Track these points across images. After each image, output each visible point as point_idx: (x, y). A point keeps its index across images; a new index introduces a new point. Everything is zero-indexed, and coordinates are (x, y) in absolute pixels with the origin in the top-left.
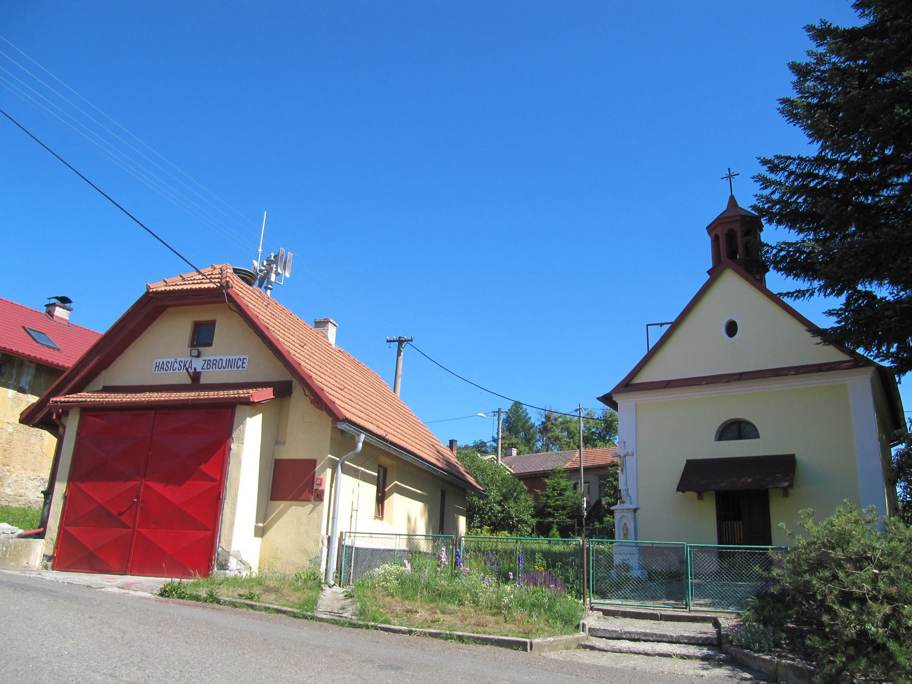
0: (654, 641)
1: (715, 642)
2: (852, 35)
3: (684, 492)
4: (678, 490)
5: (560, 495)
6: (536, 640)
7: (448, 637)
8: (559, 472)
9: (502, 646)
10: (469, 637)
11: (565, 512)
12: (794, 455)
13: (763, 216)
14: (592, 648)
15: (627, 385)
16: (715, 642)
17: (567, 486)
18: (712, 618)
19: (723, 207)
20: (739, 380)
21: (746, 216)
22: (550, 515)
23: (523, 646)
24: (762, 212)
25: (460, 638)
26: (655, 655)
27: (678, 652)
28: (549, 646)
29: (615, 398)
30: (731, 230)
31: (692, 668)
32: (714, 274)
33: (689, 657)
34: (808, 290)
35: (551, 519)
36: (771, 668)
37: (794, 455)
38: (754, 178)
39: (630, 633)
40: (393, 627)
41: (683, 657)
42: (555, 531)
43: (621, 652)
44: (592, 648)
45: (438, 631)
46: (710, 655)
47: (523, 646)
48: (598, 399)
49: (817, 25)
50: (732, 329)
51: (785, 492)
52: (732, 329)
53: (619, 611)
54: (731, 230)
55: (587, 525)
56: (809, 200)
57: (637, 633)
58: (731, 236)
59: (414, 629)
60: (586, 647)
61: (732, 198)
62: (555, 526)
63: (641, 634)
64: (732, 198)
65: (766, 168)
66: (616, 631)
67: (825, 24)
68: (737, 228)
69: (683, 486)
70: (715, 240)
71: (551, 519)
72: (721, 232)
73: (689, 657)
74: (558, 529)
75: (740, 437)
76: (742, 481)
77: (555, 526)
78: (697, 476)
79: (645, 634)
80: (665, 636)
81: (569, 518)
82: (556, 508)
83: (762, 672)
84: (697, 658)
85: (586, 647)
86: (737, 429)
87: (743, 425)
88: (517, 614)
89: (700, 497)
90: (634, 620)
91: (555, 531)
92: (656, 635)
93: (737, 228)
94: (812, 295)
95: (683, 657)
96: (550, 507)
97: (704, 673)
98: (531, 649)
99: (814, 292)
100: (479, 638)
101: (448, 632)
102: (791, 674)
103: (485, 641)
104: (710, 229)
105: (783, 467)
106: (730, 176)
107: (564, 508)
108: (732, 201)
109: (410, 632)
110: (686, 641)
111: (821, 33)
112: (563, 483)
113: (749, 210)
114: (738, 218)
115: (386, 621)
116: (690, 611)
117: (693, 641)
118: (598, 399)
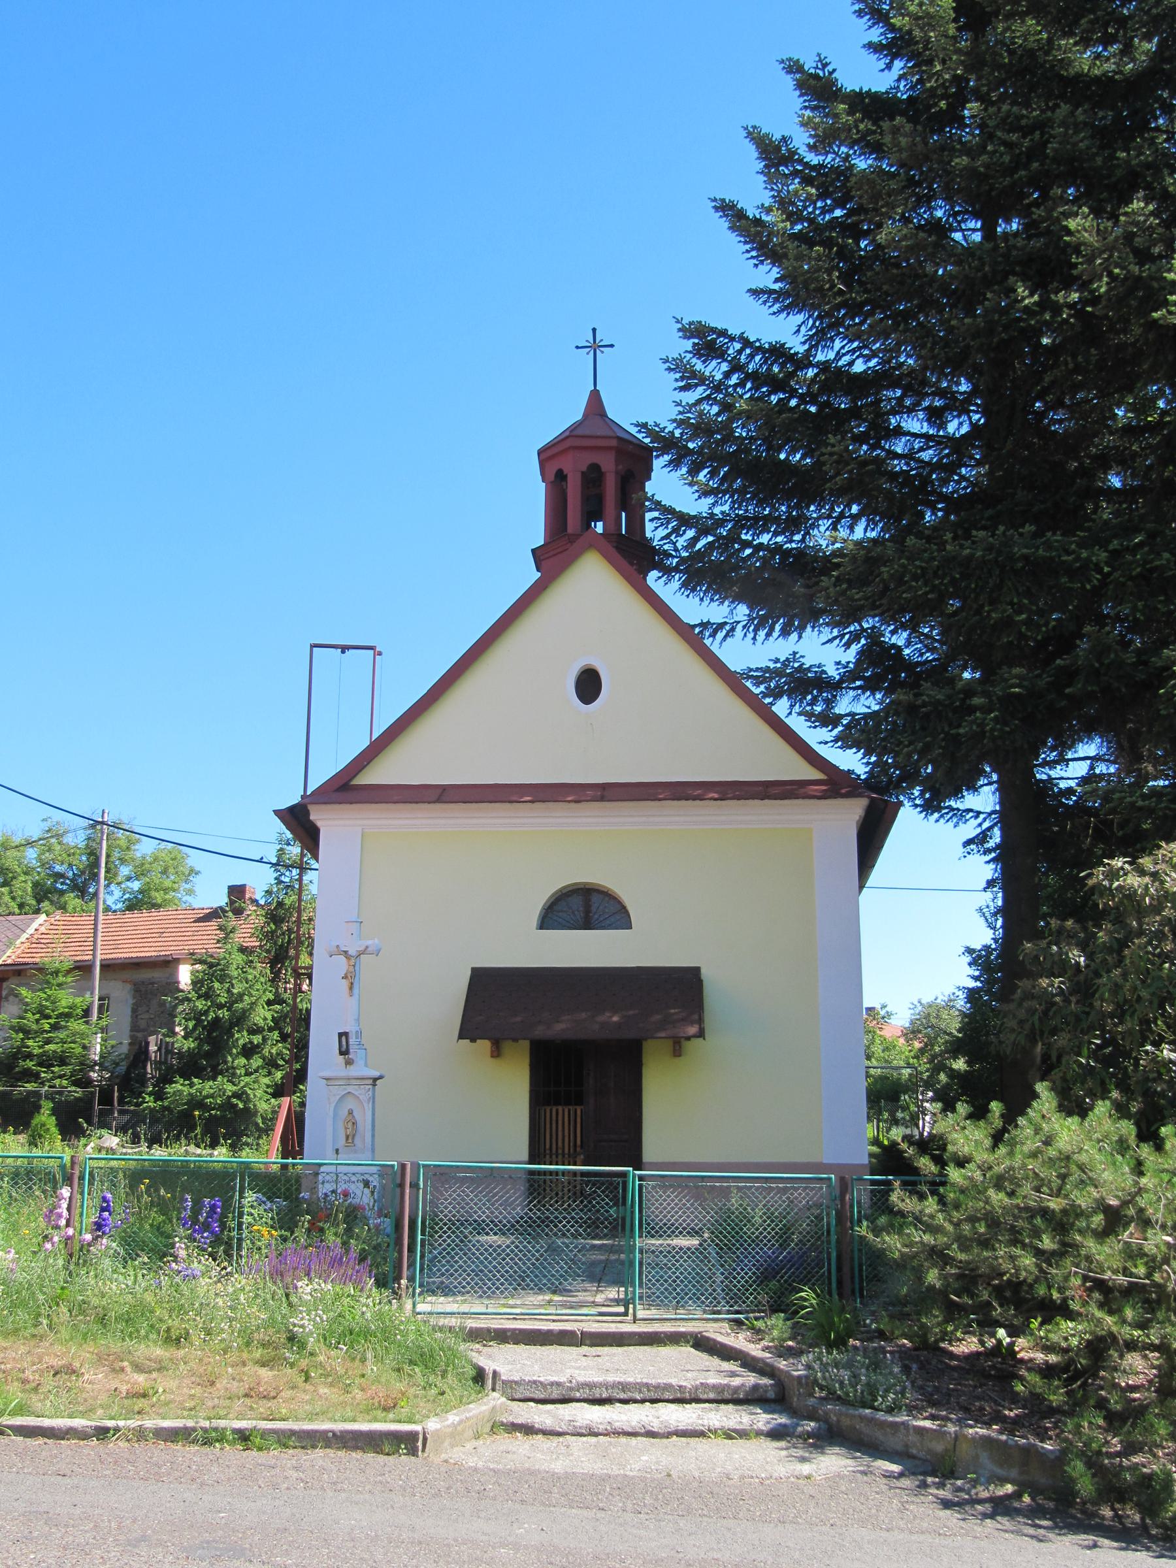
0: (643, 1401)
1: (771, 1395)
2: (872, 106)
3: (473, 1040)
4: (461, 1036)
5: (55, 1027)
6: (432, 1425)
7: (210, 1438)
8: (56, 973)
9: (356, 1448)
10: (265, 1434)
11: (67, 1070)
12: (697, 970)
13: (664, 451)
14: (528, 1430)
15: (344, 788)
16: (771, 1395)
17: (72, 1007)
18: (691, 1334)
19: (575, 413)
20: (602, 799)
21: (630, 442)
22: (33, 1076)
23: (408, 1443)
24: (667, 444)
25: (244, 1437)
26: (668, 1435)
27: (717, 1424)
28: (452, 1435)
29: (317, 815)
30: (595, 468)
31: (771, 1461)
32: (552, 559)
33: (742, 1434)
34: (721, 626)
35: (30, 1087)
36: (939, 1447)
37: (697, 970)
38: (666, 361)
39: (590, 1386)
40: (46, 1422)
41: (729, 1434)
42: (46, 1118)
43: (596, 1435)
44: (528, 1430)
45: (178, 1423)
46: (785, 1426)
47: (408, 1443)
48: (276, 812)
49: (810, 65)
50: (588, 685)
51: (677, 1050)
52: (588, 685)
53: (488, 1330)
54: (595, 468)
55: (121, 1101)
56: (777, 440)
57: (606, 1386)
58: (593, 478)
59: (110, 1423)
60: (514, 1428)
61: (595, 398)
62: (47, 1106)
63: (615, 1385)
64: (595, 398)
65: (688, 344)
66: (558, 1384)
67: (825, 65)
68: (608, 464)
69: (469, 1030)
70: (556, 483)
71: (30, 1087)
72: (575, 467)
73: (742, 1434)
74: (54, 1112)
75: (587, 923)
76: (601, 1018)
77: (47, 1106)
78: (496, 1004)
79: (624, 1387)
80: (668, 1387)
81: (75, 1083)
82: (46, 1061)
83: (914, 1457)
84: (759, 1433)
85: (514, 1428)
86: (582, 907)
87: (595, 898)
88: (334, 1358)
89: (496, 1053)
90: (521, 1348)
91: (46, 1118)
92: (647, 1385)
93: (608, 464)
94: (730, 633)
95: (729, 1434)
96: (29, 1056)
97: (806, 1469)
98: (423, 1450)
99: (733, 629)
100: (293, 1433)
101: (206, 1424)
102: (984, 1458)
103: (310, 1440)
104: (547, 455)
105: (675, 997)
106: (595, 347)
107: (62, 1061)
108: (595, 402)
109: (102, 1433)
110: (712, 1396)
111: (818, 87)
112: (65, 999)
113: (633, 430)
114: (614, 443)
115: (20, 1410)
116: (635, 1320)
117: (727, 1396)
118: (276, 812)
